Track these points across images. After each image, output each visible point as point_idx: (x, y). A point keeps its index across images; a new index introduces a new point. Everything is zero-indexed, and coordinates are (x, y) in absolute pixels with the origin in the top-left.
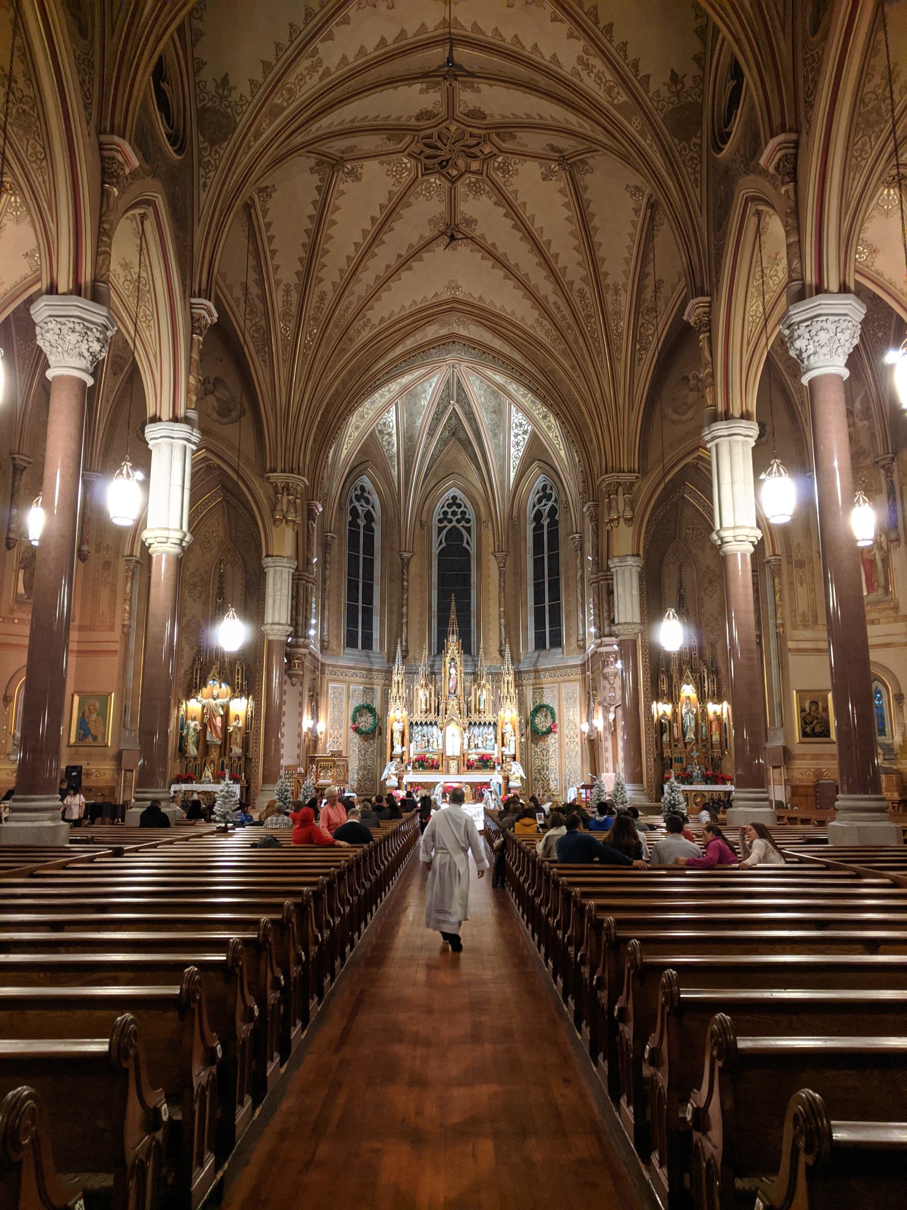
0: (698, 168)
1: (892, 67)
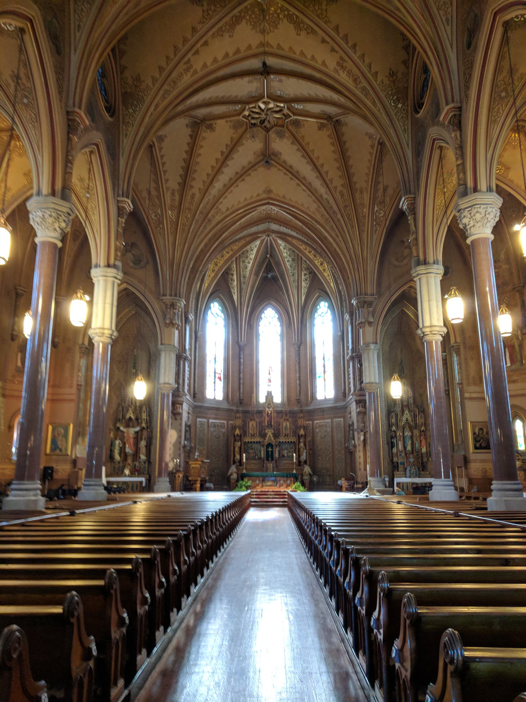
0: (406, 122)
1: (512, 66)
